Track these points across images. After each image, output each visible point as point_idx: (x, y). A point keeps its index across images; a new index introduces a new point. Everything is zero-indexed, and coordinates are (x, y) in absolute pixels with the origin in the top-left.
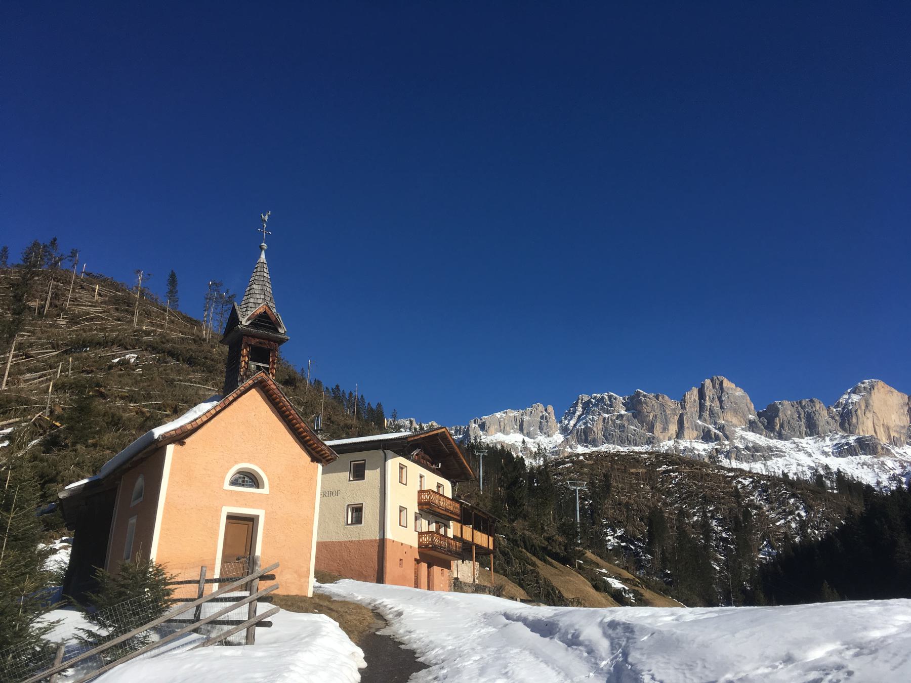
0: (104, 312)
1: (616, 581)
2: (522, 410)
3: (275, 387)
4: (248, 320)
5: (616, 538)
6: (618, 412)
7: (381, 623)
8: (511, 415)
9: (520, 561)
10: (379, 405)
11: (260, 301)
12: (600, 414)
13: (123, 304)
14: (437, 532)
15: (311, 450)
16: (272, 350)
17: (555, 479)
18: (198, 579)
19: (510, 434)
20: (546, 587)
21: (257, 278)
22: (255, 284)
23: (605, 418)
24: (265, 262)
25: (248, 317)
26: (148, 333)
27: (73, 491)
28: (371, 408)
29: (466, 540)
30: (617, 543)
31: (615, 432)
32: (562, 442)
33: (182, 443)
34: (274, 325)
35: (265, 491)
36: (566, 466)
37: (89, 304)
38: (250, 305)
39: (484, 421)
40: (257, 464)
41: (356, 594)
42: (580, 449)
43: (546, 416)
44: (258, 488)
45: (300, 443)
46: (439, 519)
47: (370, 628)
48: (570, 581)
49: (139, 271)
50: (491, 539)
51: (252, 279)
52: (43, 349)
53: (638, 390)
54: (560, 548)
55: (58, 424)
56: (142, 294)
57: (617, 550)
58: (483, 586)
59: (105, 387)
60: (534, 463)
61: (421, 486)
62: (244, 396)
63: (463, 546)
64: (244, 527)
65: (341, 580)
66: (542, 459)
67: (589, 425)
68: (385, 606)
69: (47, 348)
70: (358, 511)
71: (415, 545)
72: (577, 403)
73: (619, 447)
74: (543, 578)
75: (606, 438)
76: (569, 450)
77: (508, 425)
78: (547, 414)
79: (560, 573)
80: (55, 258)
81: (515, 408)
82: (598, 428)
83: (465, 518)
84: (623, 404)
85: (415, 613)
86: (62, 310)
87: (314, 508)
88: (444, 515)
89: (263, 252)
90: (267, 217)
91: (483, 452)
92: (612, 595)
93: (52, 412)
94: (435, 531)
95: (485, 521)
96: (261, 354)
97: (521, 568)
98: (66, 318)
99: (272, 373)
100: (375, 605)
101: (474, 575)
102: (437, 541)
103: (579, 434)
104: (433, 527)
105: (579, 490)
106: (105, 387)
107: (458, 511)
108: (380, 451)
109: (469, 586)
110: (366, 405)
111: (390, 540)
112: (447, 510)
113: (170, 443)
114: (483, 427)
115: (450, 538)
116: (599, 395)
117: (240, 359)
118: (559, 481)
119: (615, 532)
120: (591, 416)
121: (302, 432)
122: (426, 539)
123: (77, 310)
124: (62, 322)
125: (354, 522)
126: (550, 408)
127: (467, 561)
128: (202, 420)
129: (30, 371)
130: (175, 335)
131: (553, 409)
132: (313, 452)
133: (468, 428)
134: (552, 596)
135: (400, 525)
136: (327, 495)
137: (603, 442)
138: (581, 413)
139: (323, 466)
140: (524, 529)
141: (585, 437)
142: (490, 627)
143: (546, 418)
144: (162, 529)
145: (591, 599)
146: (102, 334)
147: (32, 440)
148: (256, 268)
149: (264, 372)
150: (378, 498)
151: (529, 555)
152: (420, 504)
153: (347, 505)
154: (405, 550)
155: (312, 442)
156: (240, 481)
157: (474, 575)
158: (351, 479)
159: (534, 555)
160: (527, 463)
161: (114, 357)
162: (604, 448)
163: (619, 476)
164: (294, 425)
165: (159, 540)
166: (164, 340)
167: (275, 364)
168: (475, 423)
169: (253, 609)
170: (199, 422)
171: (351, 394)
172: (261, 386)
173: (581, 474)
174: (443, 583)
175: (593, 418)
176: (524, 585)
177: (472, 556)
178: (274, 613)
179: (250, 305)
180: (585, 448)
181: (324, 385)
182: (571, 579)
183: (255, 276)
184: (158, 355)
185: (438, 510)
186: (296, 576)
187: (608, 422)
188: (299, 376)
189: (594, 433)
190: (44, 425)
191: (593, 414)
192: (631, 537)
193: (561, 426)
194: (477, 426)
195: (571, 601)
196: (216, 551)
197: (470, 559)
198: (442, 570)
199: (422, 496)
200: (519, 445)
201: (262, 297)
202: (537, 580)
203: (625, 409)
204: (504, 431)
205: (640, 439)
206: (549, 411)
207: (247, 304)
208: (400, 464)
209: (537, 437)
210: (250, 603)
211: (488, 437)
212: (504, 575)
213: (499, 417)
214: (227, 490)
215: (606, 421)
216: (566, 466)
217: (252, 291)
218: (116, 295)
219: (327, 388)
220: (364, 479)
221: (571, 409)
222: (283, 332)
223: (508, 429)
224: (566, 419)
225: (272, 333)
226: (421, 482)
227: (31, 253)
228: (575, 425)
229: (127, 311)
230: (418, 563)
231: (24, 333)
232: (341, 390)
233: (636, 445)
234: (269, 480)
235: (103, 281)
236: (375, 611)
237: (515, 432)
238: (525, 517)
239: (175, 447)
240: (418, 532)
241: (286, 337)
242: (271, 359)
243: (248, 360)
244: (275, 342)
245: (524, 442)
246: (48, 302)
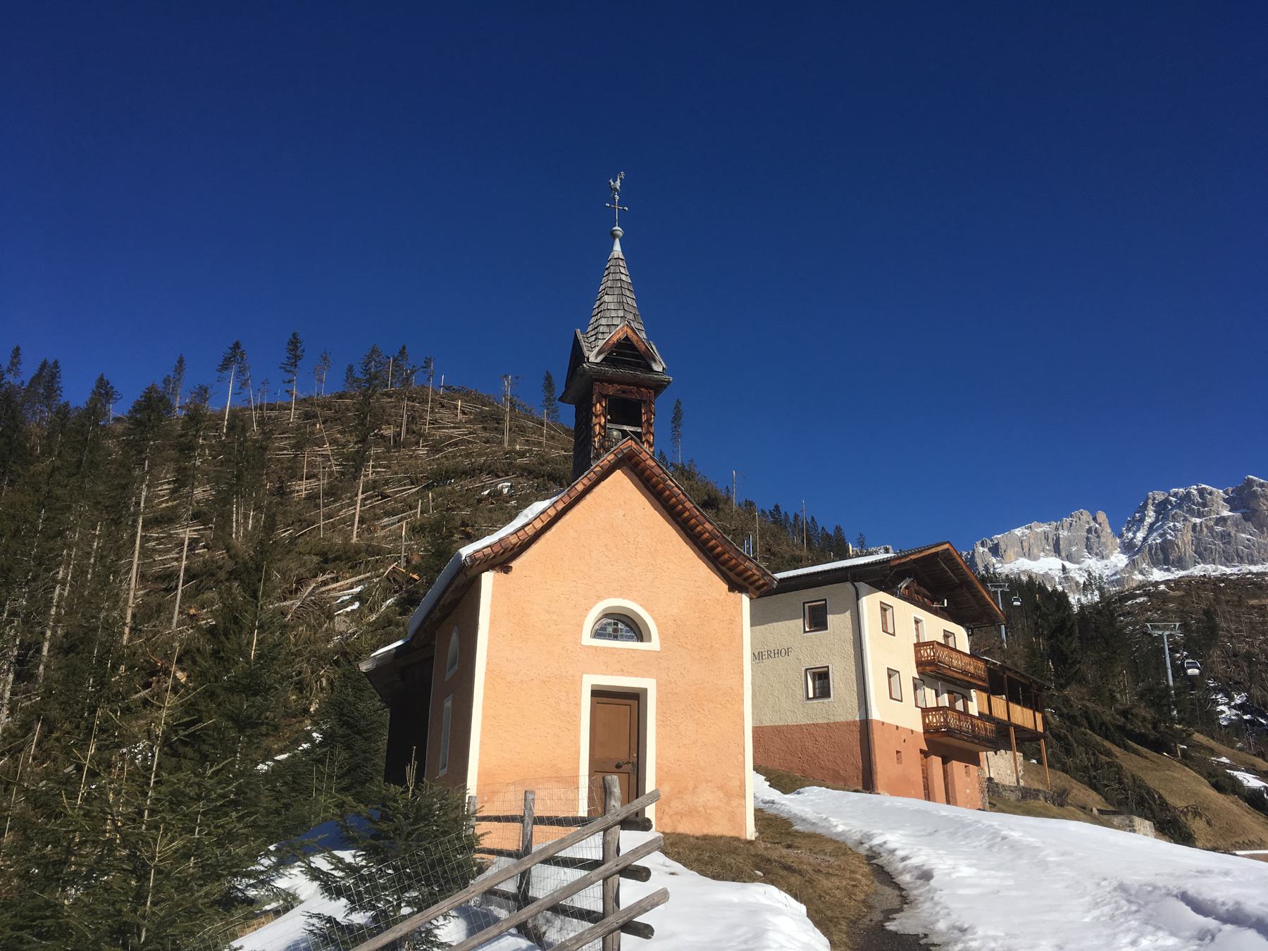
0: (470, 433)
1: (1248, 776)
3: (654, 464)
4: (599, 353)
5: (1234, 707)
7: (889, 896)
8: (1039, 530)
9: (1086, 749)
10: (838, 529)
13: (492, 420)
14: (952, 707)
15: (727, 571)
16: (645, 402)
17: (1121, 621)
18: (519, 812)
19: (1038, 559)
20: (1138, 790)
21: (609, 284)
22: (607, 294)
23: (1195, 525)
24: (622, 257)
25: (597, 349)
26: (522, 454)
27: (380, 659)
28: (827, 534)
29: (997, 719)
30: (1237, 715)
31: (1215, 544)
32: (1127, 566)
33: (506, 569)
34: (644, 359)
35: (654, 644)
36: (1138, 601)
37: (452, 425)
38: (601, 329)
39: (996, 542)
40: (635, 600)
41: (834, 820)
42: (1157, 575)
44: (642, 641)
45: (706, 560)
46: (952, 687)
47: (871, 907)
48: (1174, 778)
49: (506, 376)
50: (1039, 716)
51: (602, 287)
52: (401, 486)
54: (1145, 727)
55: (415, 577)
56: (513, 405)
57: (1236, 728)
58: (1035, 790)
59: (473, 526)
60: (1083, 600)
61: (918, 636)
62: (603, 484)
63: (997, 728)
64: (622, 711)
65: (807, 788)
66: (1096, 592)
67: (1169, 537)
68: (892, 852)
69: (405, 485)
70: (822, 677)
71: (919, 729)
72: (1146, 505)
73: (1224, 568)
74: (1129, 775)
75: (1200, 555)
76: (1140, 577)
77: (1035, 545)
78: (1097, 526)
79: (1154, 766)
80: (406, 370)
81: (1043, 520)
82: (1185, 541)
83: (994, 684)
84: (1225, 500)
85: (958, 874)
86: (421, 435)
87: (742, 673)
88: (958, 679)
89: (617, 241)
90: (618, 183)
91: (1001, 587)
92: (1245, 797)
93: (408, 561)
94: (947, 705)
95: (1026, 689)
96: (625, 411)
97: (1089, 759)
98: (426, 446)
99: (648, 442)
100: (871, 847)
101: (1016, 771)
102: (953, 722)
103: (1153, 552)
104: (945, 700)
105: (1167, 636)
106: (473, 526)
107: (983, 674)
108: (848, 585)
109: (1011, 791)
110: (820, 529)
111: (878, 721)
112: (965, 673)
113: (487, 570)
114: (995, 550)
115: (974, 717)
116: (1181, 490)
118: (1129, 624)
119: (1232, 699)
120: (1172, 524)
121: (708, 540)
122: (933, 719)
123: (438, 434)
124: (422, 452)
125: (817, 695)
126: (1102, 516)
127: (1003, 751)
128: (534, 528)
129: (388, 514)
130: (554, 454)
133: (973, 554)
134: (1149, 803)
135: (891, 698)
136: (772, 654)
137: (1195, 562)
138: (1153, 519)
139: (751, 599)
140: (1083, 699)
141: (1164, 555)
142: (1160, 934)
144: (485, 717)
145: (1213, 806)
146: (467, 462)
147: (385, 600)
148: (607, 269)
149: (632, 439)
150: (852, 656)
151: (1098, 738)
152: (919, 664)
153: (803, 669)
154: (903, 737)
155: (726, 556)
156: (610, 630)
157: (1016, 771)
158: (807, 629)
159: (1106, 738)
160: (1073, 599)
161: (483, 488)
162: (1197, 570)
163: (1229, 611)
164: (693, 528)
165: (481, 737)
166: (542, 461)
167: (651, 425)
168: (983, 545)
169: (611, 894)
170: (530, 531)
171: (796, 516)
172: (630, 463)
173: (1165, 612)
174: (971, 787)
175: (1174, 525)
176: (1098, 786)
177: (1010, 744)
178: (657, 905)
179: (601, 329)
180: (1166, 573)
181: (759, 506)
182: (1176, 775)
183: (607, 282)
184: (536, 480)
185: (950, 673)
186: (721, 795)
187: (1201, 530)
188: (723, 494)
189: (1179, 548)
190: (399, 579)
191: (1174, 519)
192: (1258, 704)
193: (1123, 542)
194: (986, 550)
195: (1182, 812)
196: (578, 753)
197: (1008, 747)
198: (966, 767)
199: (922, 652)
200: (1057, 574)
201: (621, 313)
202: (1120, 779)
203: (1229, 508)
204: (1030, 555)
205: (1259, 553)
206: (1099, 520)
207: (596, 328)
208: (881, 602)
210: (605, 880)
211: (1006, 566)
212: (1063, 771)
213: (1019, 534)
214: (587, 647)
215: (1198, 528)
216: (1138, 601)
217: (603, 307)
218: (482, 411)
219: (762, 511)
220: (826, 629)
221: (1137, 515)
222: (660, 369)
223: (1035, 551)
224: (1128, 530)
225: (641, 372)
226: (917, 629)
227: (370, 362)
228: (1145, 539)
229: (496, 429)
230: (926, 757)
231: (379, 469)
232: (783, 513)
233: (1252, 562)
234: (658, 626)
235: (467, 396)
236: (874, 861)
237: (1047, 555)
238: (1082, 680)
240: (922, 708)
242: (644, 418)
243: (605, 422)
244: (647, 388)
245: (1064, 569)
246: (404, 428)
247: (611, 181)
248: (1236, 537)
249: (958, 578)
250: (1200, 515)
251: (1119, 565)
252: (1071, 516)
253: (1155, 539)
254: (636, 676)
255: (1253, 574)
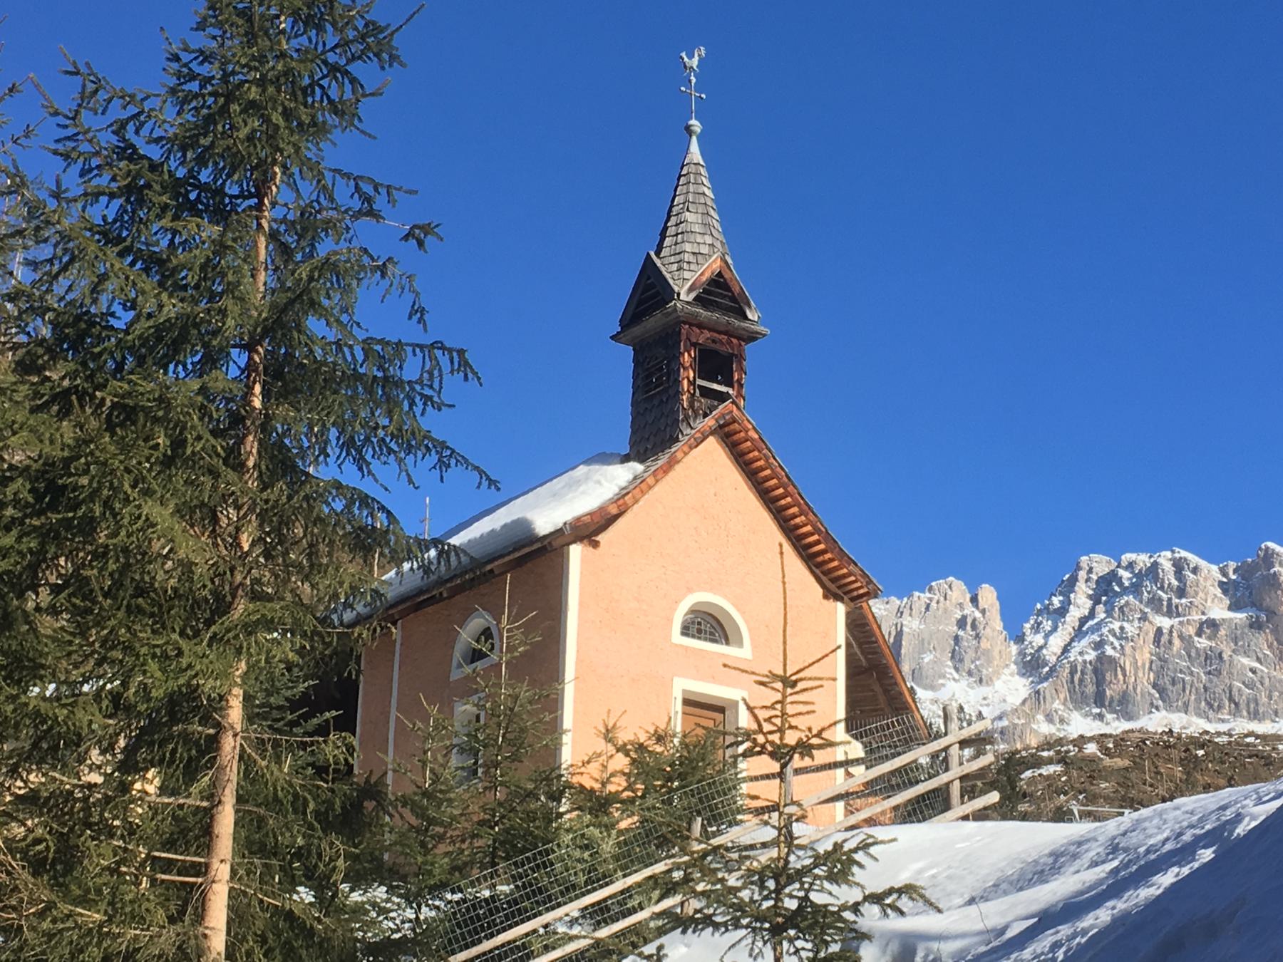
2: (901, 598)
4: (691, 290)
6: (1203, 613)
11: (705, 250)
12: (1144, 618)
15: (821, 575)
23: (1159, 631)
24: (702, 163)
31: (1192, 674)
32: (1024, 702)
33: (596, 545)
38: (687, 257)
40: (725, 597)
43: (974, 620)
44: (727, 643)
53: (1271, 545)
67: (1109, 651)
72: (1074, 580)
75: (1162, 691)
78: (978, 615)
84: (1221, 584)
89: (694, 139)
113: (574, 542)
117: (679, 375)
120: (1116, 625)
126: (988, 595)
131: (998, 598)
132: (824, 578)
143: (974, 627)
162: (1156, 722)
172: (728, 436)
175: (1122, 628)
180: (1098, 723)
187: (1170, 642)
189: (1124, 675)
193: (1022, 653)
206: (982, 603)
209: (943, 685)
214: (676, 645)
215: (1165, 638)
217: (682, 228)
224: (1037, 628)
228: (1066, 650)
233: (1255, 716)
239: (582, 551)
241: (760, 328)
243: (694, 378)
244: (739, 338)
247: (683, 55)
248: (1231, 662)
249: (865, 658)
250: (1171, 612)
251: (1010, 699)
252: (931, 589)
253: (1084, 652)
254: (727, 685)
255: (1257, 737)
